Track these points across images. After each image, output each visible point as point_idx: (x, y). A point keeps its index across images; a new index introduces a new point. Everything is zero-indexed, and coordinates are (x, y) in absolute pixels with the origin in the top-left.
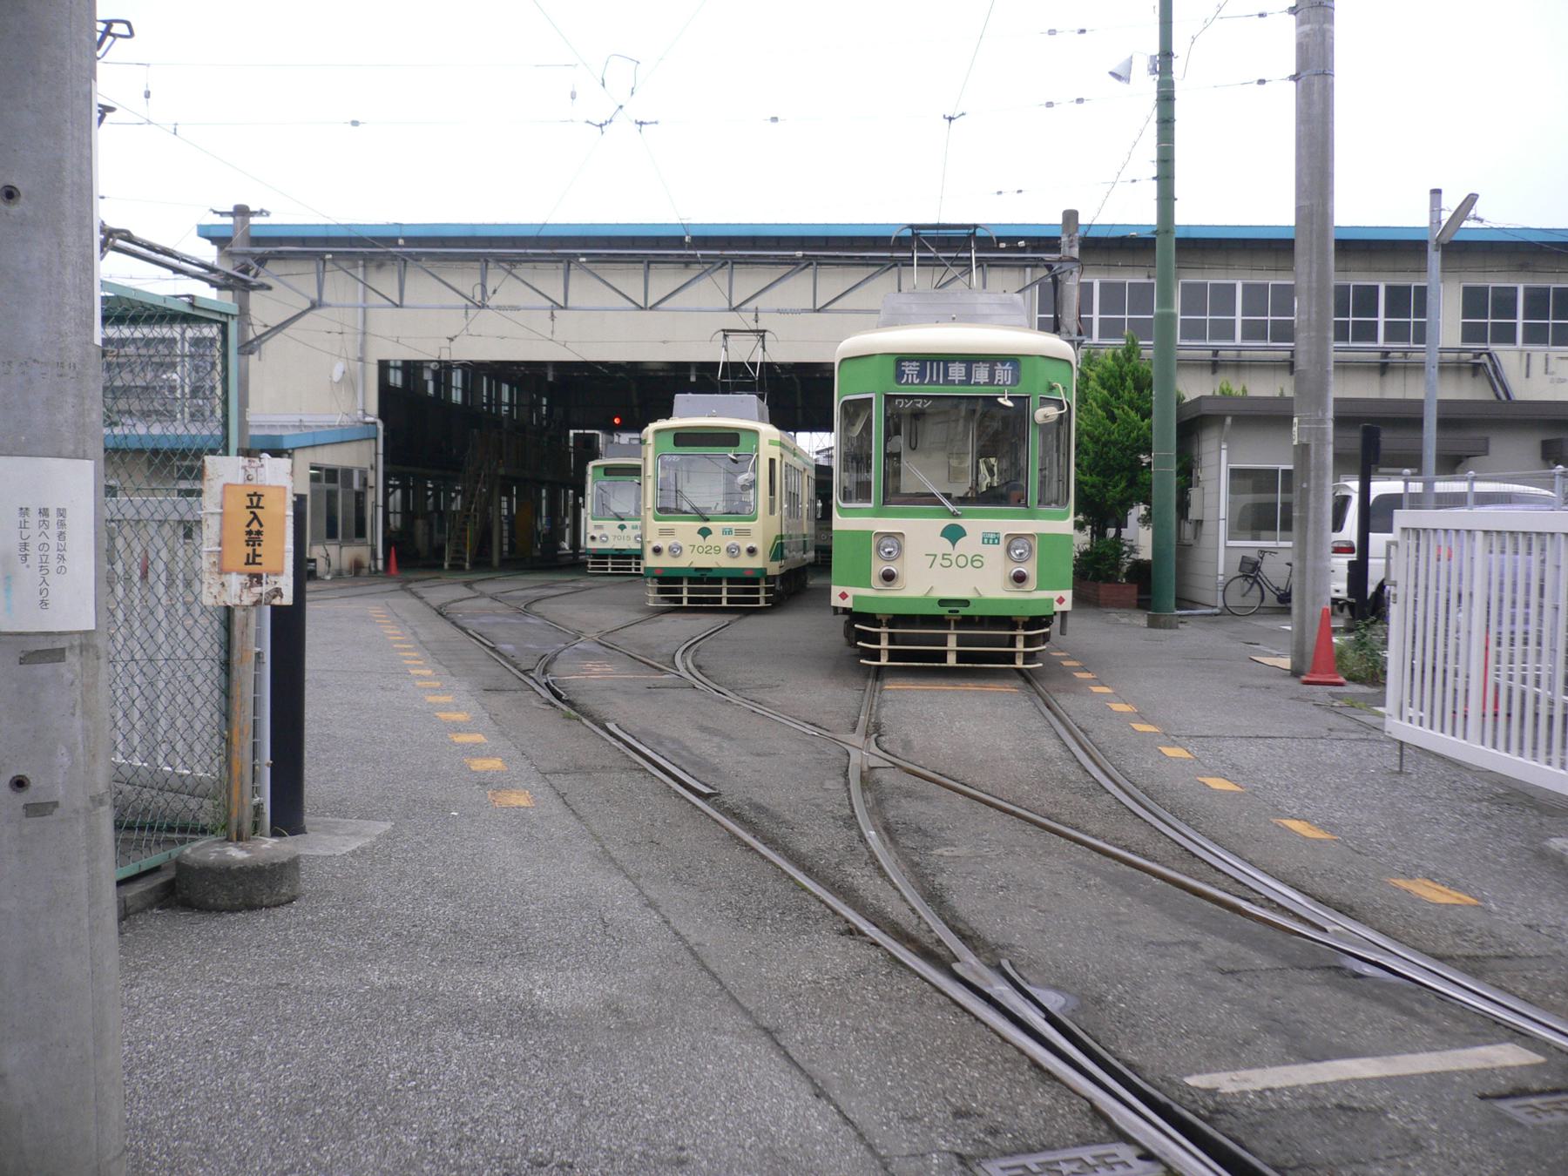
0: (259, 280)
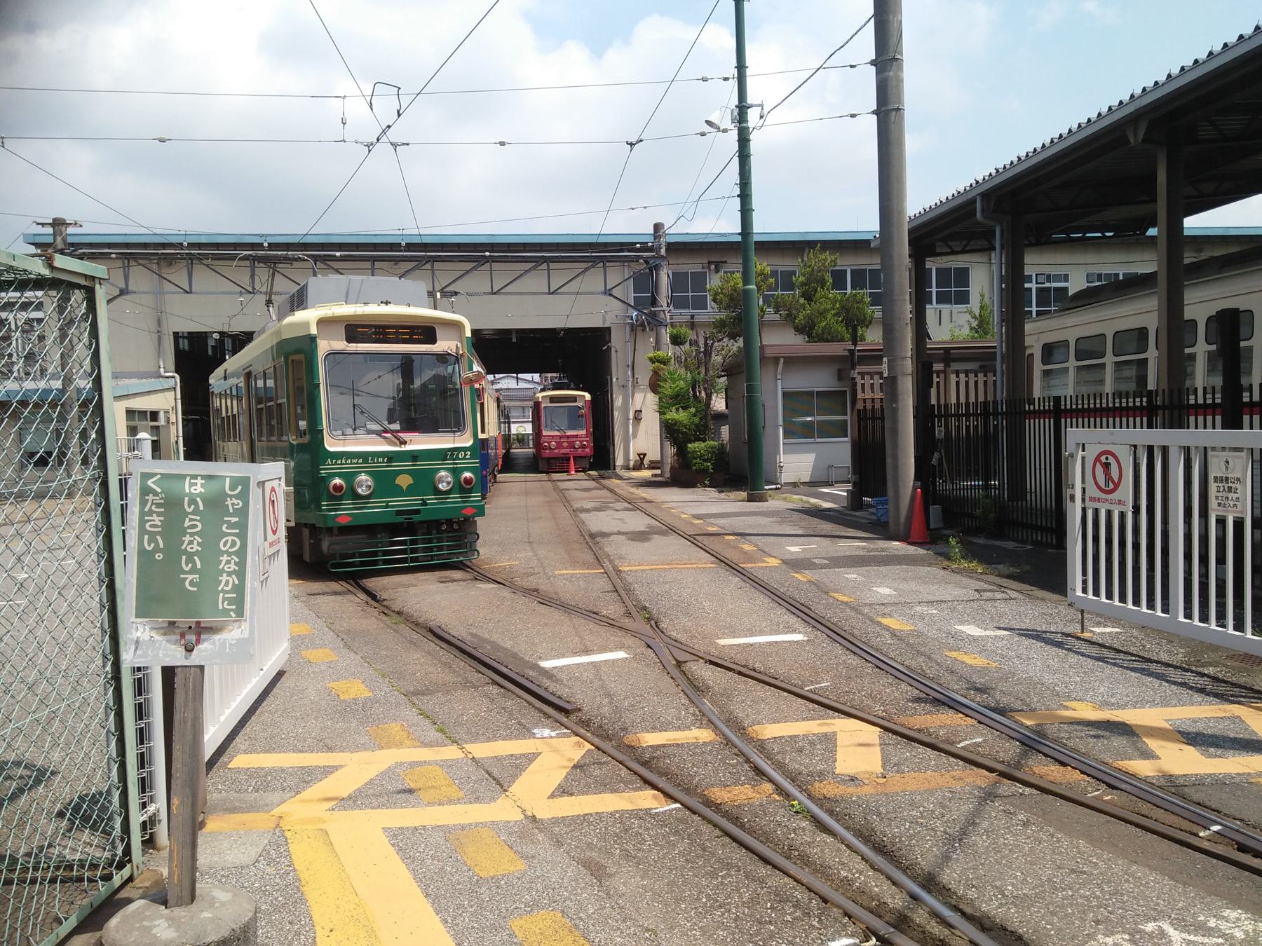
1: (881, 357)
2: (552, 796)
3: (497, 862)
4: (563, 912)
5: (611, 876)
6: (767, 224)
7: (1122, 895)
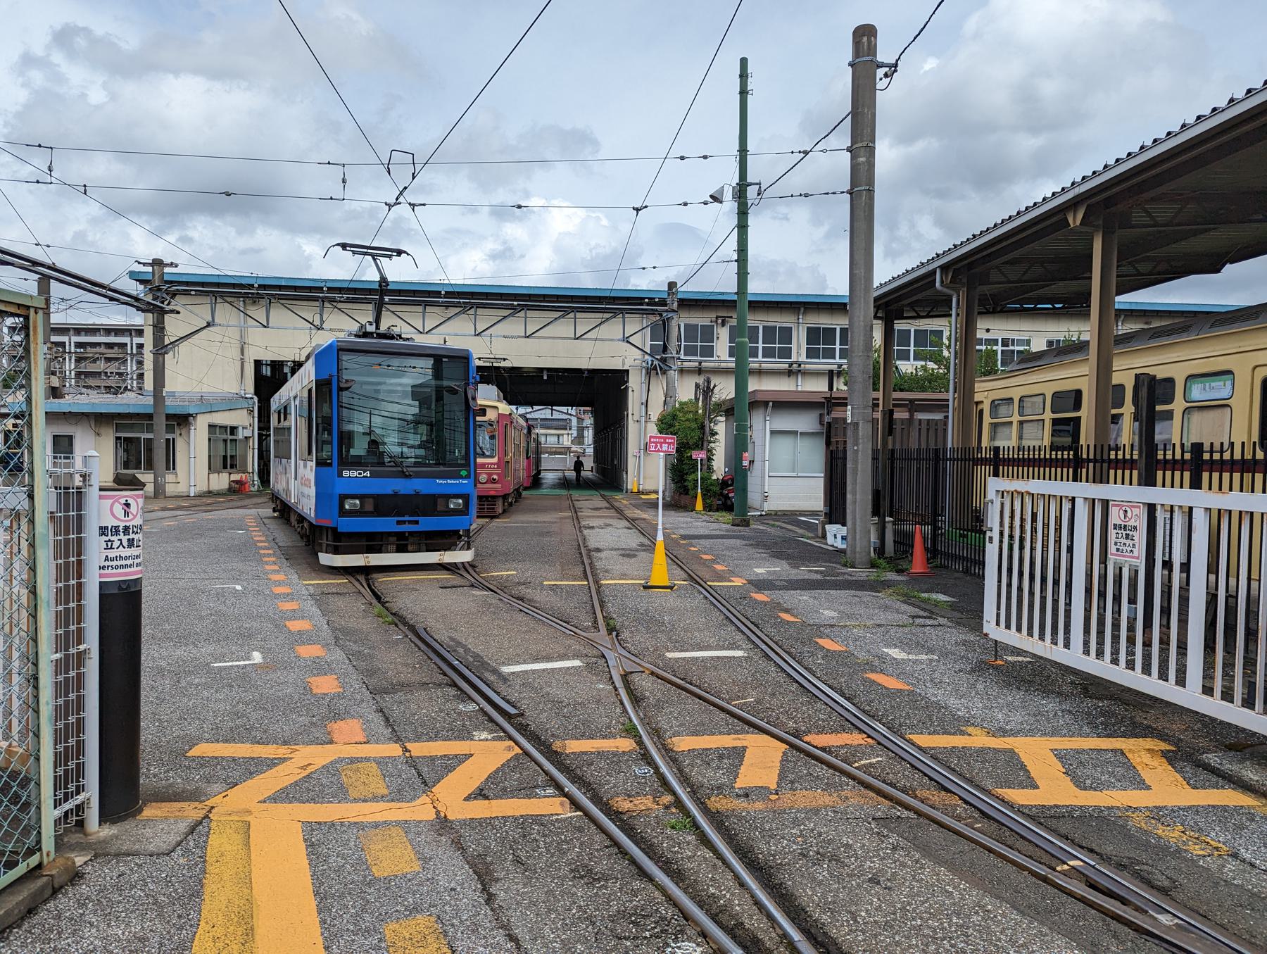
1: (846, 405)
2: (467, 799)
3: (393, 860)
4: (438, 917)
5: (497, 880)
6: (756, 287)
7: (968, 928)
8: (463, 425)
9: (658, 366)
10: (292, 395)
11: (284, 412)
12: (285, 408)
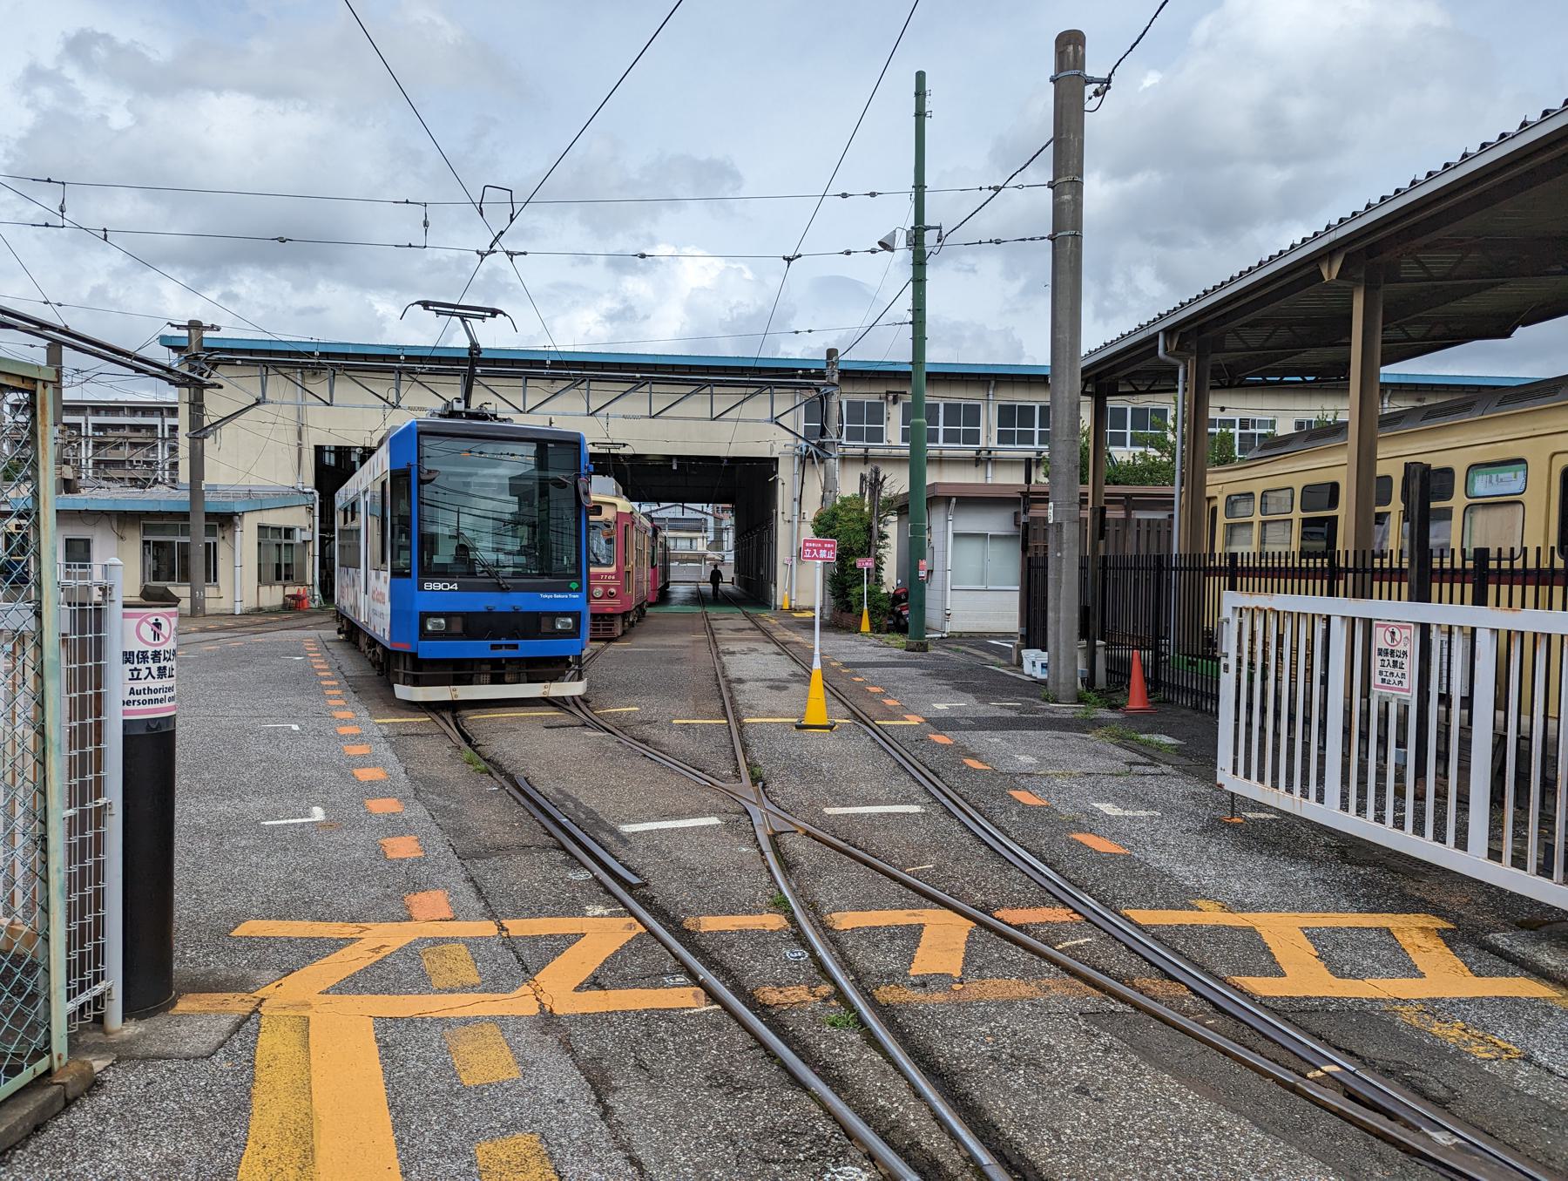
0: (211, 381)
1: (1047, 501)
2: (578, 989)
3: (486, 1064)
4: (543, 1135)
5: (615, 1089)
6: (936, 355)
7: (1198, 1148)
8: (573, 526)
9: (814, 454)
10: (362, 488)
11: (351, 510)
12: (353, 505)
